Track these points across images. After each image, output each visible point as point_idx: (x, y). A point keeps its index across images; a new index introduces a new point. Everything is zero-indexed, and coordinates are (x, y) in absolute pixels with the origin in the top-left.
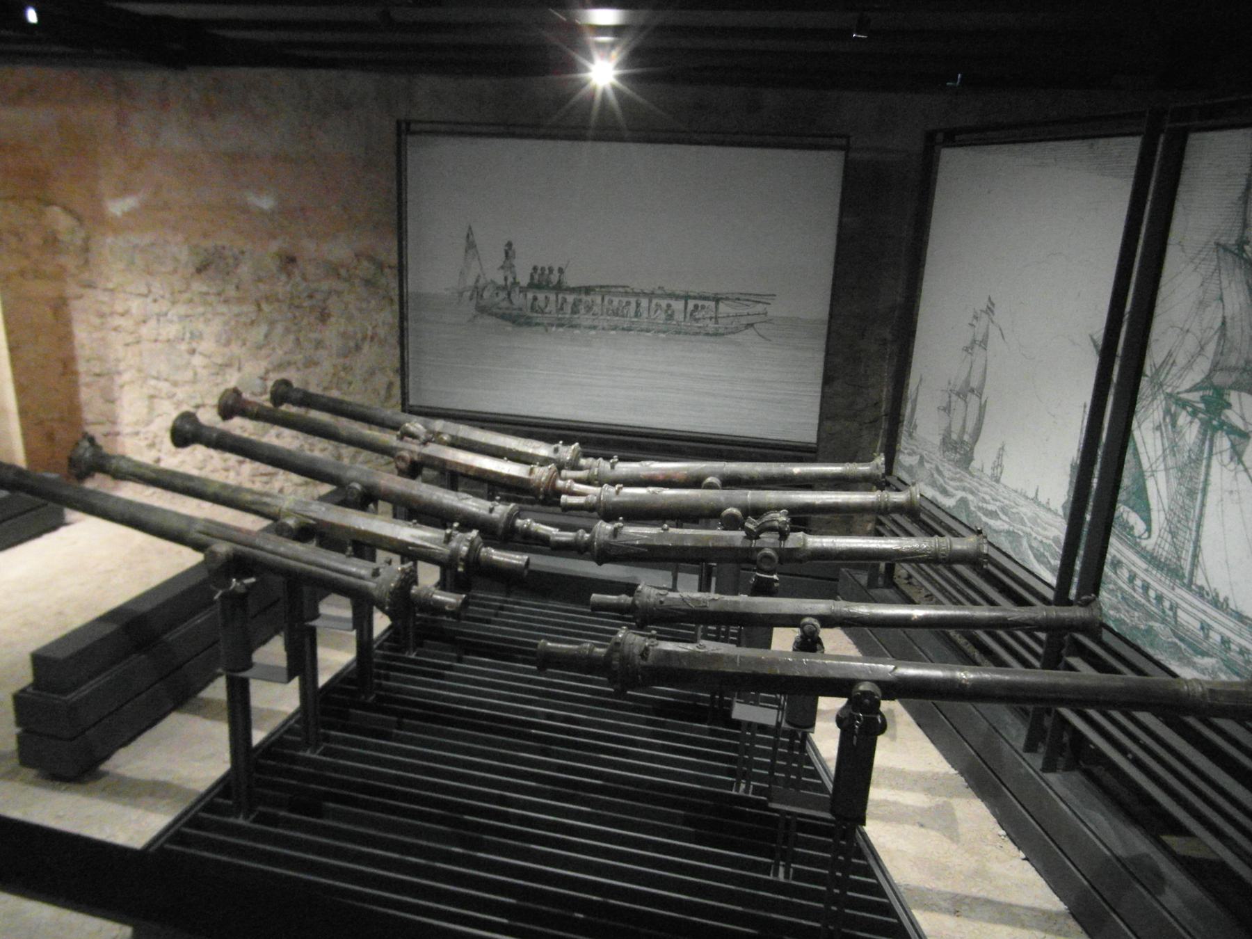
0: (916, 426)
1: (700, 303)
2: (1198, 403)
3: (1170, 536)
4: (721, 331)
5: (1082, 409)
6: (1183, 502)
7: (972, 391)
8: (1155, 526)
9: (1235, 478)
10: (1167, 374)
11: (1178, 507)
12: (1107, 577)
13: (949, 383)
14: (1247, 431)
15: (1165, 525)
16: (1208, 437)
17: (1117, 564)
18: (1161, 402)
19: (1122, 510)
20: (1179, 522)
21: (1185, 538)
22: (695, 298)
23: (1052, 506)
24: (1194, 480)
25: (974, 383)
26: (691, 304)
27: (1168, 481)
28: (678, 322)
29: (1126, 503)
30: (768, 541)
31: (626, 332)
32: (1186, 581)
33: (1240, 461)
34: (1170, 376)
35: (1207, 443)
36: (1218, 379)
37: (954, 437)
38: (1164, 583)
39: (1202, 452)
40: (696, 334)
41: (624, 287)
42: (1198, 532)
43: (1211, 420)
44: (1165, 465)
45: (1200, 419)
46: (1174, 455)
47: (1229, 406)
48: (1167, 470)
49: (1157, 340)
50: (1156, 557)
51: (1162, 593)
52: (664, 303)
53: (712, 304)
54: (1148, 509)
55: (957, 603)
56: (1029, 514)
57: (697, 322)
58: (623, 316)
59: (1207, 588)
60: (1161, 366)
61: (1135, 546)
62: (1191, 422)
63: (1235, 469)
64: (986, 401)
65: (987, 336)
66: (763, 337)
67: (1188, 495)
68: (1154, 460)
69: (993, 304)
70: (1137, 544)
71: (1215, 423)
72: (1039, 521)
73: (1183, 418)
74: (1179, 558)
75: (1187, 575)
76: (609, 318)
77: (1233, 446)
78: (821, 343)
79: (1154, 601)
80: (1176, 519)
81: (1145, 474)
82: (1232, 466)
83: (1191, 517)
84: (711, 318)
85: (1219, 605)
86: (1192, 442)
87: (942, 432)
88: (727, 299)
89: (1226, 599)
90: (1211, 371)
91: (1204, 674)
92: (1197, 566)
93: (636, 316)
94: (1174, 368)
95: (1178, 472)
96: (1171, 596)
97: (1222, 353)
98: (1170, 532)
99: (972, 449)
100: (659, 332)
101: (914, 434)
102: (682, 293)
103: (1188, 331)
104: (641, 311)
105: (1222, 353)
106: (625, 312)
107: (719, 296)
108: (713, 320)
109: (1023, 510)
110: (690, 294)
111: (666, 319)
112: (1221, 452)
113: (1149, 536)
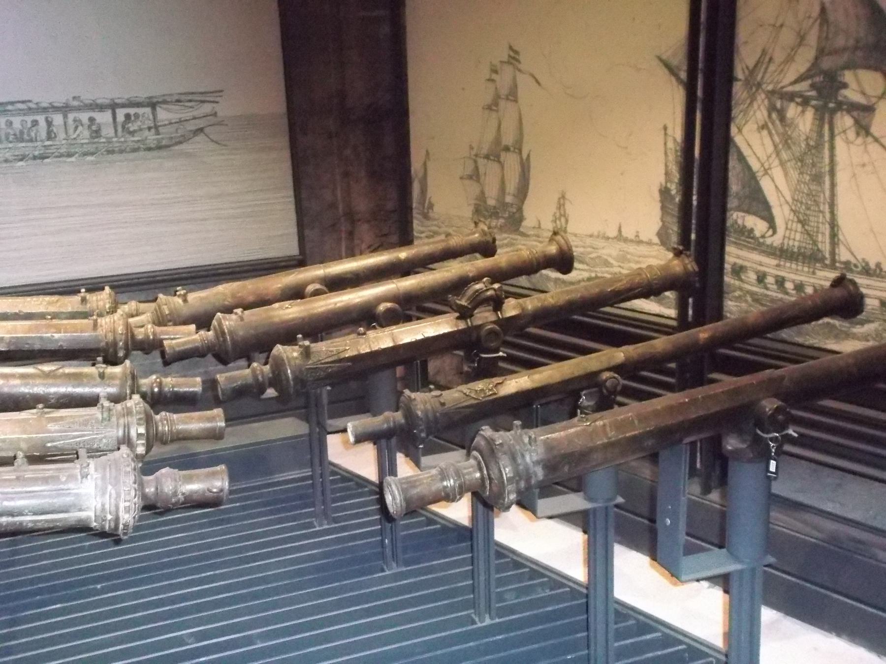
0: (431, 206)
1: (132, 111)
3: (799, 226)
4: (164, 143)
5: (663, 132)
6: (809, 189)
7: (507, 149)
8: (779, 222)
9: (866, 151)
10: (765, 72)
11: (805, 195)
12: (729, 285)
13: (471, 148)
14: (870, 104)
15: (791, 218)
16: (826, 120)
17: (738, 271)
18: (763, 101)
19: (737, 217)
20: (808, 209)
21: (818, 222)
22: (123, 106)
23: (644, 237)
24: (818, 165)
25: (508, 139)
26: (121, 114)
27: (786, 174)
28: (107, 138)
29: (739, 209)
30: (484, 317)
31: (39, 161)
32: (828, 262)
33: (868, 133)
34: (768, 75)
35: (826, 127)
36: (827, 63)
37: (491, 202)
38: (797, 270)
39: (820, 135)
40: (135, 150)
41: (23, 102)
42: (832, 213)
43: (825, 106)
44: (781, 161)
45: (813, 107)
46: (789, 148)
47: (845, 86)
48: (782, 164)
51: (801, 281)
52: (84, 117)
53: (148, 110)
54: (767, 207)
55: (530, 365)
56: (614, 253)
57: (133, 136)
58: (31, 141)
59: (853, 261)
60: (756, 66)
61: (758, 246)
62: (803, 112)
63: (864, 142)
64: (529, 156)
65: (516, 86)
66: (216, 142)
67: (813, 181)
68: (765, 158)
69: (516, 52)
70: (760, 244)
71: (831, 105)
72: (629, 256)
73: (792, 111)
74: (815, 243)
75: (827, 255)
76: (10, 145)
77: (857, 122)
78: (284, 141)
79: (794, 292)
80: (804, 207)
81: (757, 174)
82: (860, 140)
84: (149, 128)
85: (871, 272)
86: (808, 130)
87: (473, 202)
88: (165, 102)
89: (878, 265)
90: (817, 58)
91: (868, 341)
92: (838, 244)
93: (49, 138)
94: (771, 65)
95: (797, 162)
96: (812, 280)
97: (827, 38)
98: (799, 221)
99: (520, 209)
100: (85, 154)
101: (431, 214)
102: (107, 102)
103: (782, 26)
104: (55, 130)
105: (827, 38)
106: (33, 134)
107: (155, 100)
108: (153, 131)
109: (604, 251)
110: (117, 101)
111: (92, 137)
112: (844, 132)
113: (775, 232)
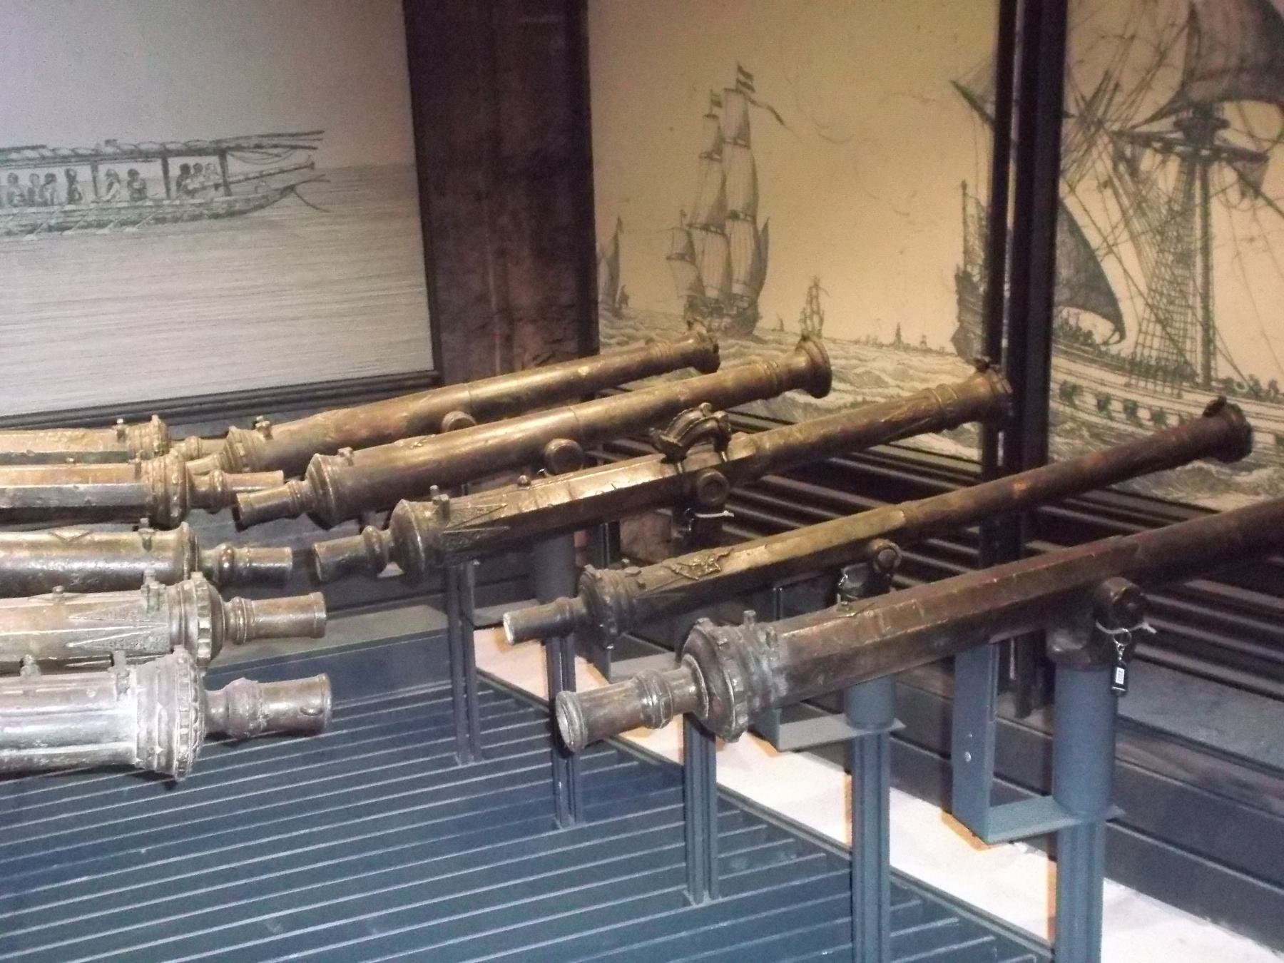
0: (625, 299)
1: (191, 161)
2: (1171, 132)
3: (1159, 327)
4: (238, 207)
5: (960, 192)
6: (1173, 274)
7: (734, 216)
8: (1129, 322)
9: (1255, 218)
10: (1109, 105)
11: (1166, 283)
12: (1057, 414)
13: (683, 215)
14: (1261, 151)
15: (1147, 316)
17: (1070, 393)
18: (1106, 146)
19: (1067, 315)
20: (1171, 303)
22: (179, 153)
23: (933, 344)
24: (1186, 239)
25: (736, 202)
26: (175, 165)
27: (1139, 253)
28: (154, 200)
29: (1071, 303)
30: (702, 459)
31: (56, 234)
32: (1199, 380)
33: (1258, 193)
34: (1112, 109)
35: (1198, 185)
36: (1198, 92)
37: (712, 293)
38: (1155, 392)
39: (1189, 195)
40: (196, 218)
41: (34, 148)
42: (1206, 308)
43: (1196, 153)
44: (1131, 233)
45: (1178, 155)
46: (1144, 214)
47: (1224, 124)
48: (1134, 238)
49: (1081, 62)
50: (1141, 362)
51: (1161, 408)
52: (122, 169)
53: (214, 160)
54: (1112, 300)
56: (890, 367)
57: (193, 197)
58: (45, 204)
59: (1236, 378)
60: (1095, 95)
61: (1099, 356)
62: (1164, 162)
63: (1253, 206)
64: (766, 226)
66: (314, 206)
67: (1178, 262)
68: (1109, 229)
69: (748, 76)
70: (1102, 354)
71: (1205, 152)
73: (1148, 160)
74: (1181, 352)
75: (1199, 370)
76: (15, 211)
77: (1242, 177)
78: (411, 205)
80: (1164, 300)
81: (1097, 253)
82: (1246, 203)
83: (1191, 289)
84: (217, 186)
85: (1263, 394)
86: (1171, 189)
87: (686, 293)
88: (239, 148)
89: (1273, 385)
90: (1183, 84)
91: (1258, 494)
92: (1214, 354)
93: (71, 200)
94: (1118, 94)
95: (1155, 235)
96: (1177, 407)
97: (1198, 55)
98: (1159, 321)
99: (754, 304)
100: (124, 223)
101: (624, 311)
102: (156, 147)
103: (1133, 37)
104: (80, 189)
105: (1198, 55)
106: (48, 195)
107: (224, 145)
108: (222, 189)
110: (169, 146)
111: (133, 199)
112: (1224, 191)
113: (1122, 337)
